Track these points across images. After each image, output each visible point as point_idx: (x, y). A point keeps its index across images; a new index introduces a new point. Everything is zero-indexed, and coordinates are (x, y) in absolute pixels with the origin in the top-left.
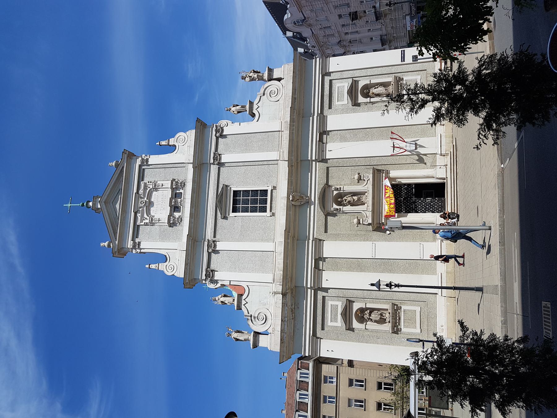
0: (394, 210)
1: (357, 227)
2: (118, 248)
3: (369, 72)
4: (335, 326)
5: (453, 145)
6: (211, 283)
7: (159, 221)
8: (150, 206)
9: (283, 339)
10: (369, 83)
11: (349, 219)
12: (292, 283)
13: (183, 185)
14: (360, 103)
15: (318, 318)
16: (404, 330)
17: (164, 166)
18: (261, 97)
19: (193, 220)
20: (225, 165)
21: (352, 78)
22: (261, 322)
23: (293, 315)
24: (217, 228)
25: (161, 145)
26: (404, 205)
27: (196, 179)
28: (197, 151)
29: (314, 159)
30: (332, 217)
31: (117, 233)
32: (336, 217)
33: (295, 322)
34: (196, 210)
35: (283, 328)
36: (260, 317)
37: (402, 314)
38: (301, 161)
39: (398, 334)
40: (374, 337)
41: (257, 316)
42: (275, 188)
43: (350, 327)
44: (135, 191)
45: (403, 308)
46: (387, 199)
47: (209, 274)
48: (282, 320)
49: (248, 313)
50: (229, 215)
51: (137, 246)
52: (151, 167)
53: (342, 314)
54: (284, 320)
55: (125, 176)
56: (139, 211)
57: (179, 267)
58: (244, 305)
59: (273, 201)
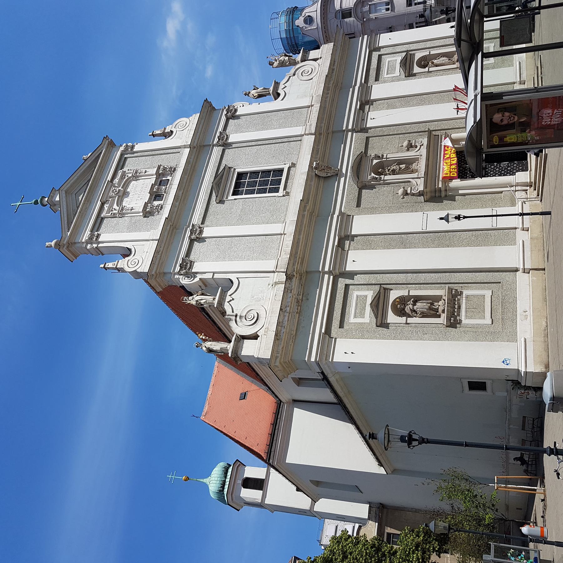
0: (456, 171)
1: (402, 198)
2: (69, 241)
3: (429, 44)
4: (360, 323)
5: (537, 67)
6: (186, 278)
7: (131, 210)
8: (124, 197)
9: (278, 335)
10: (429, 54)
11: (393, 190)
12: (302, 266)
13: (173, 170)
14: (389, 323)
15: (335, 312)
16: (465, 321)
17: (153, 153)
18: (290, 77)
19: (177, 204)
20: (232, 146)
21: (381, 284)
22: (249, 322)
23: (299, 309)
24: (208, 214)
25: (106, 269)
26: (470, 173)
27: (192, 160)
28: (199, 131)
29: (327, 269)
30: (368, 190)
31: (72, 223)
32: (374, 189)
33: (300, 317)
34: (184, 193)
35: (281, 320)
36: (250, 316)
37: (464, 301)
38: (333, 132)
39: (456, 328)
40: (419, 332)
41: (244, 315)
42: (294, 165)
43: (383, 322)
44: (109, 178)
45: (465, 293)
46: (447, 160)
47: (186, 265)
48: (281, 309)
49: (233, 312)
50: (227, 198)
51: (95, 238)
52: (135, 155)
53: (373, 303)
54: (284, 310)
55: (101, 163)
56: (108, 202)
57: (145, 262)
58: (228, 302)
59: (289, 179)
